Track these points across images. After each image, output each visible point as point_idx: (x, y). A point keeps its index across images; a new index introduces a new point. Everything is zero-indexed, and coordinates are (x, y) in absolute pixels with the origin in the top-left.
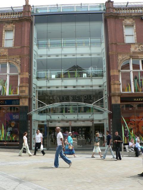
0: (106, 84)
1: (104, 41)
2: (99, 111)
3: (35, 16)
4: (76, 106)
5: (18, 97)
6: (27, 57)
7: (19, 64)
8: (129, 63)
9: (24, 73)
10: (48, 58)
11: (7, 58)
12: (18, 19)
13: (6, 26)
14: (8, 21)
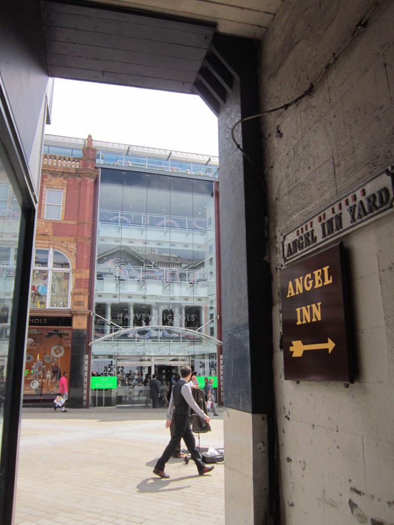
3: (102, 168)
5: (70, 312)
6: (89, 243)
7: (73, 253)
9: (83, 270)
10: (172, 248)
11: (50, 241)
12: (74, 172)
13: (50, 181)
14: (55, 171)
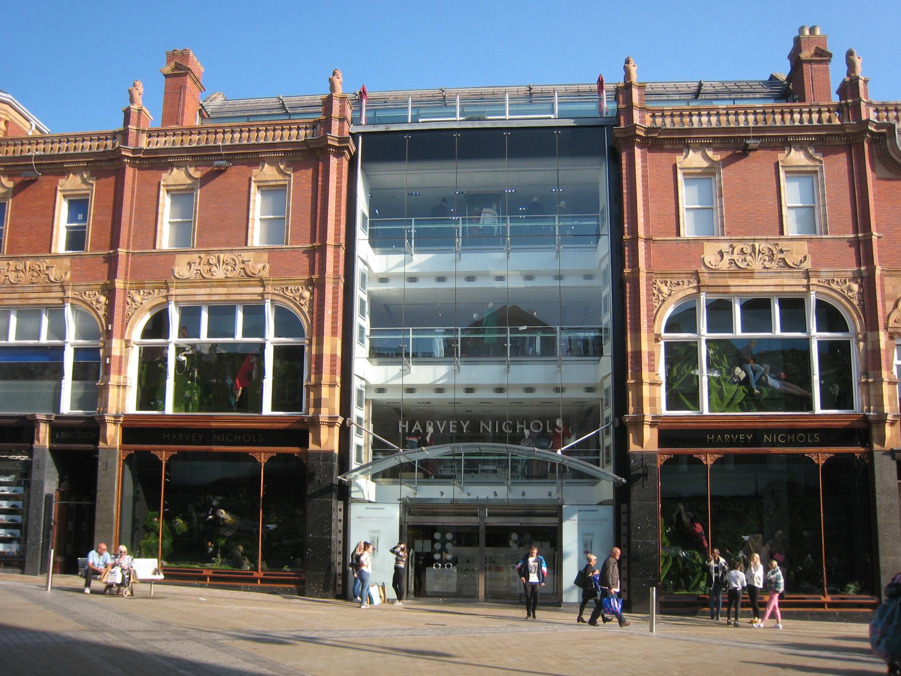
0: (609, 383)
1: (606, 229)
2: (579, 475)
8: (695, 308)
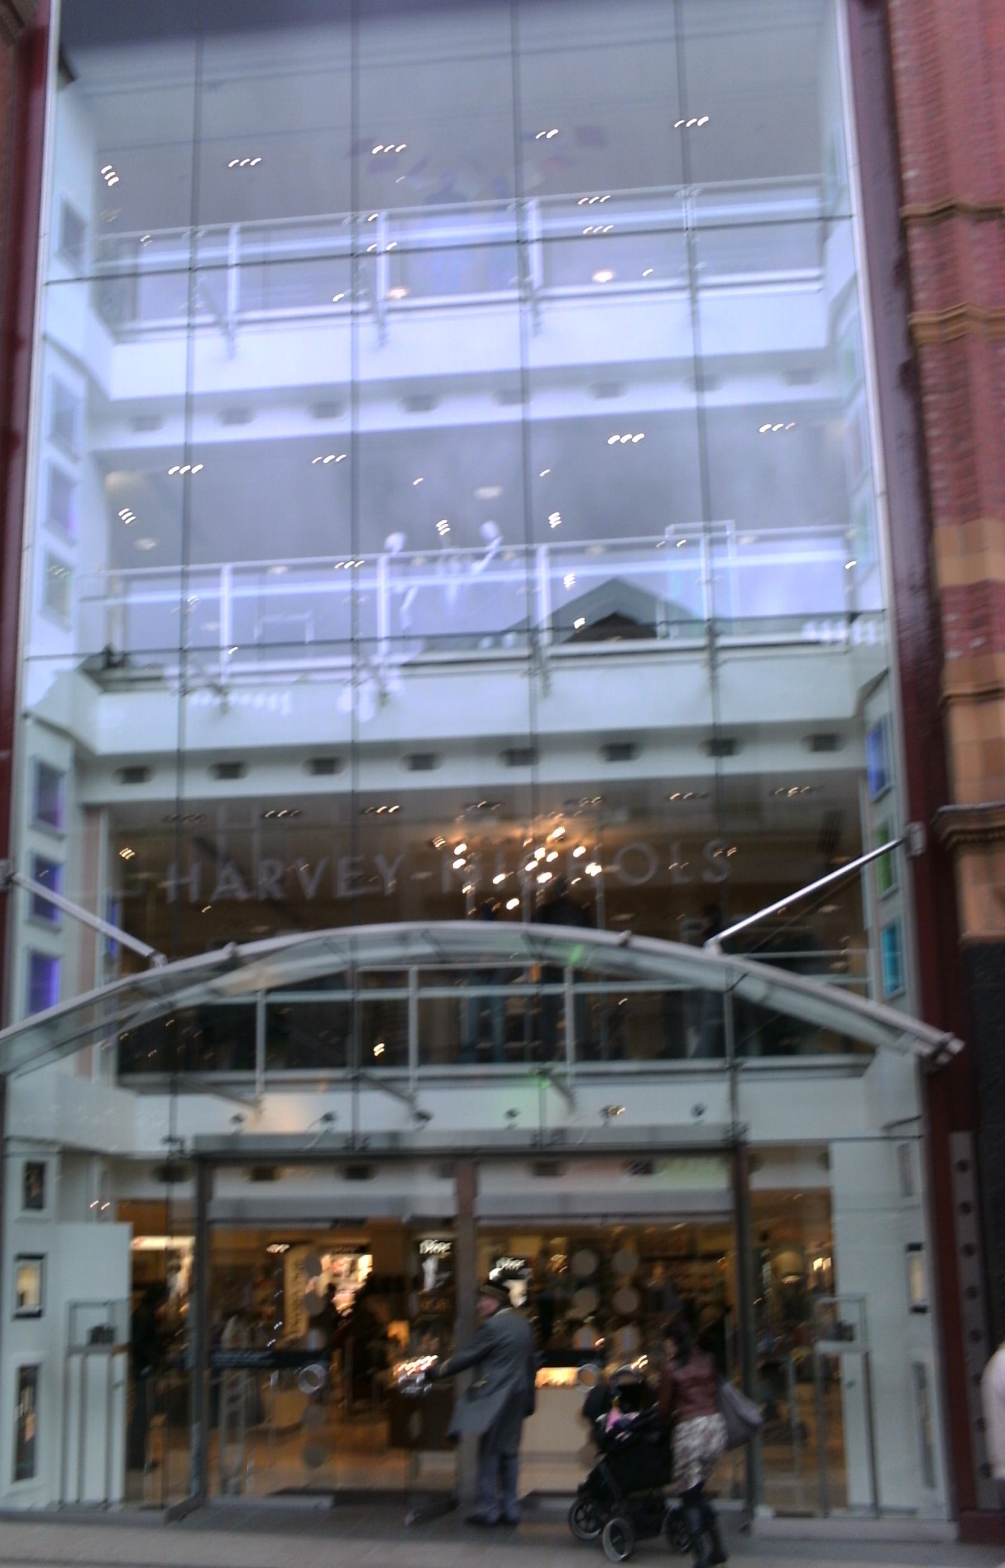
4: (511, 975)
